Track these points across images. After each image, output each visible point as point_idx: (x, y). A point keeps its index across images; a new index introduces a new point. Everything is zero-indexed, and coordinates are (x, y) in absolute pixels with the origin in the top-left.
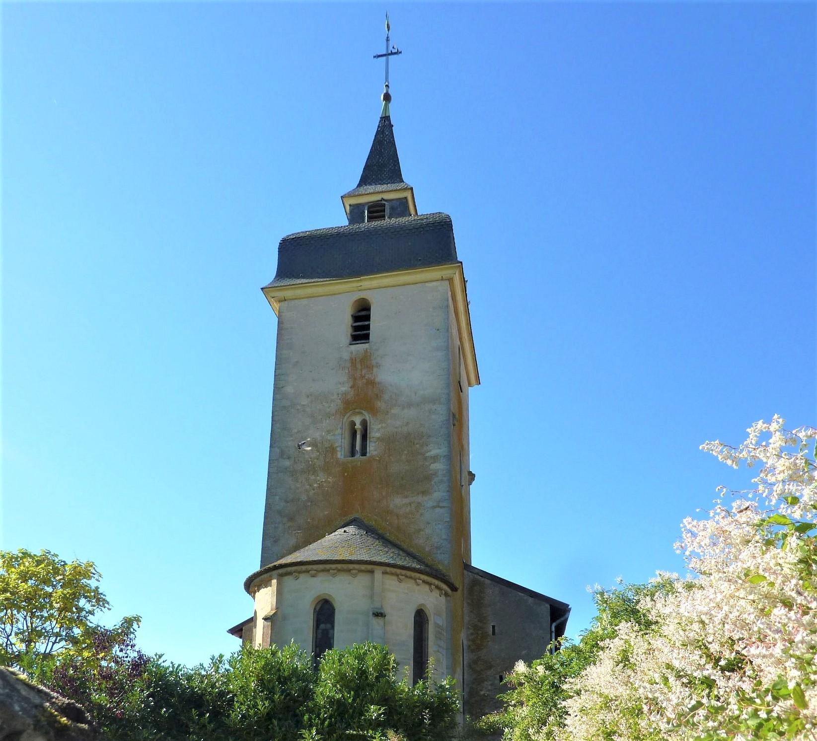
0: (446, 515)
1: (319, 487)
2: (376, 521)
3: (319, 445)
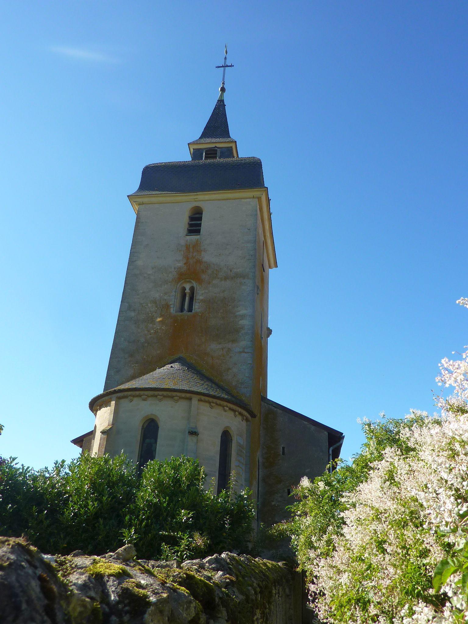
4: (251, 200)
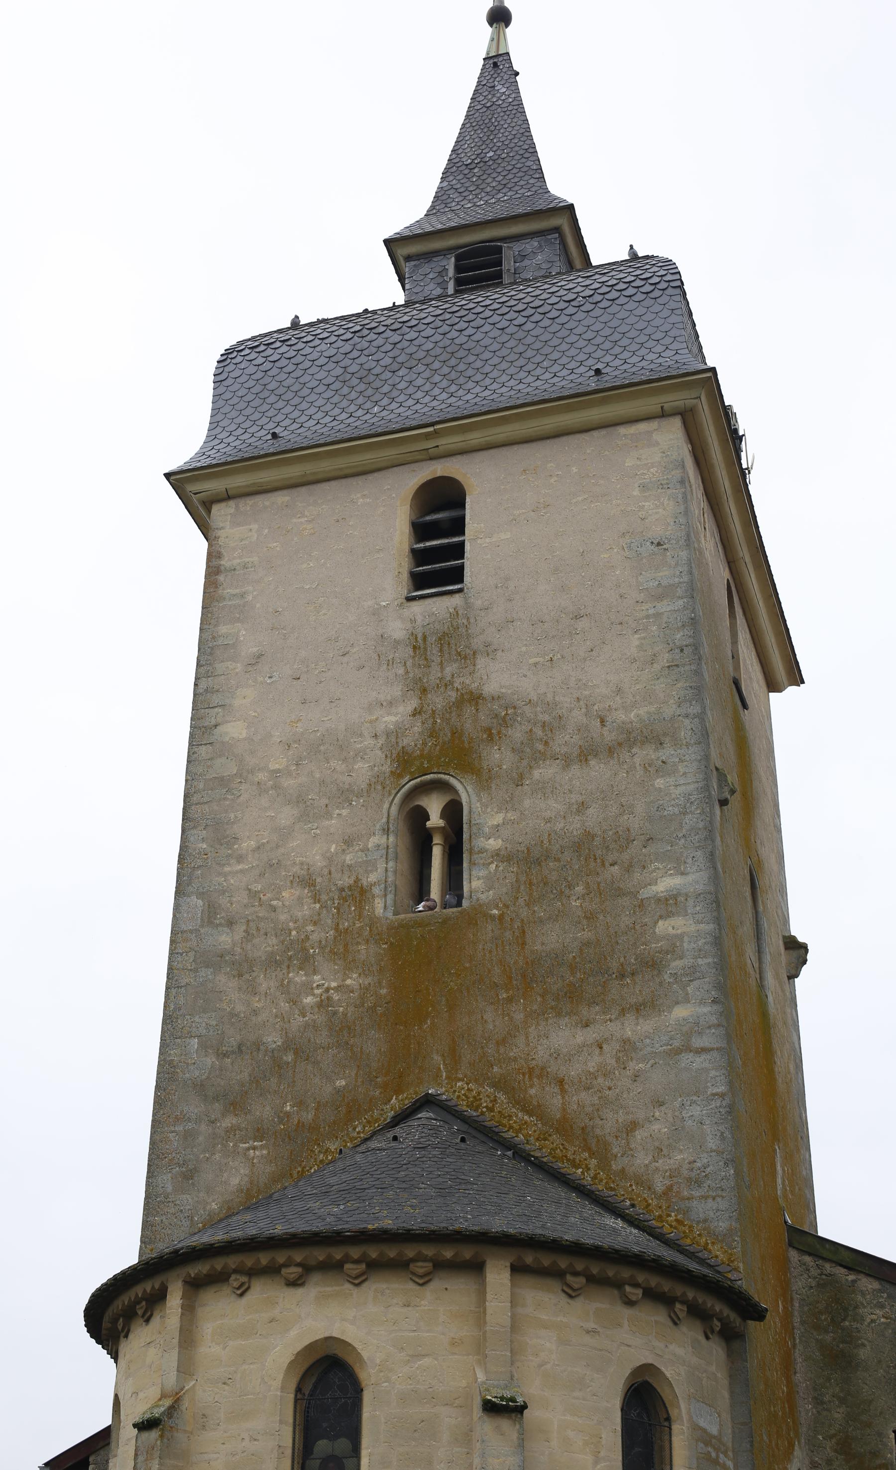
0: (713, 1073)
1: (320, 1005)
3: (319, 880)
4: (654, 424)
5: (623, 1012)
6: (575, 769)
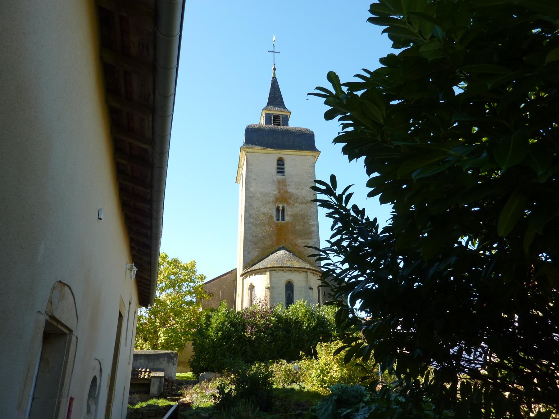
2: (291, 248)
4: (311, 157)
5: (307, 239)
6: (301, 205)
